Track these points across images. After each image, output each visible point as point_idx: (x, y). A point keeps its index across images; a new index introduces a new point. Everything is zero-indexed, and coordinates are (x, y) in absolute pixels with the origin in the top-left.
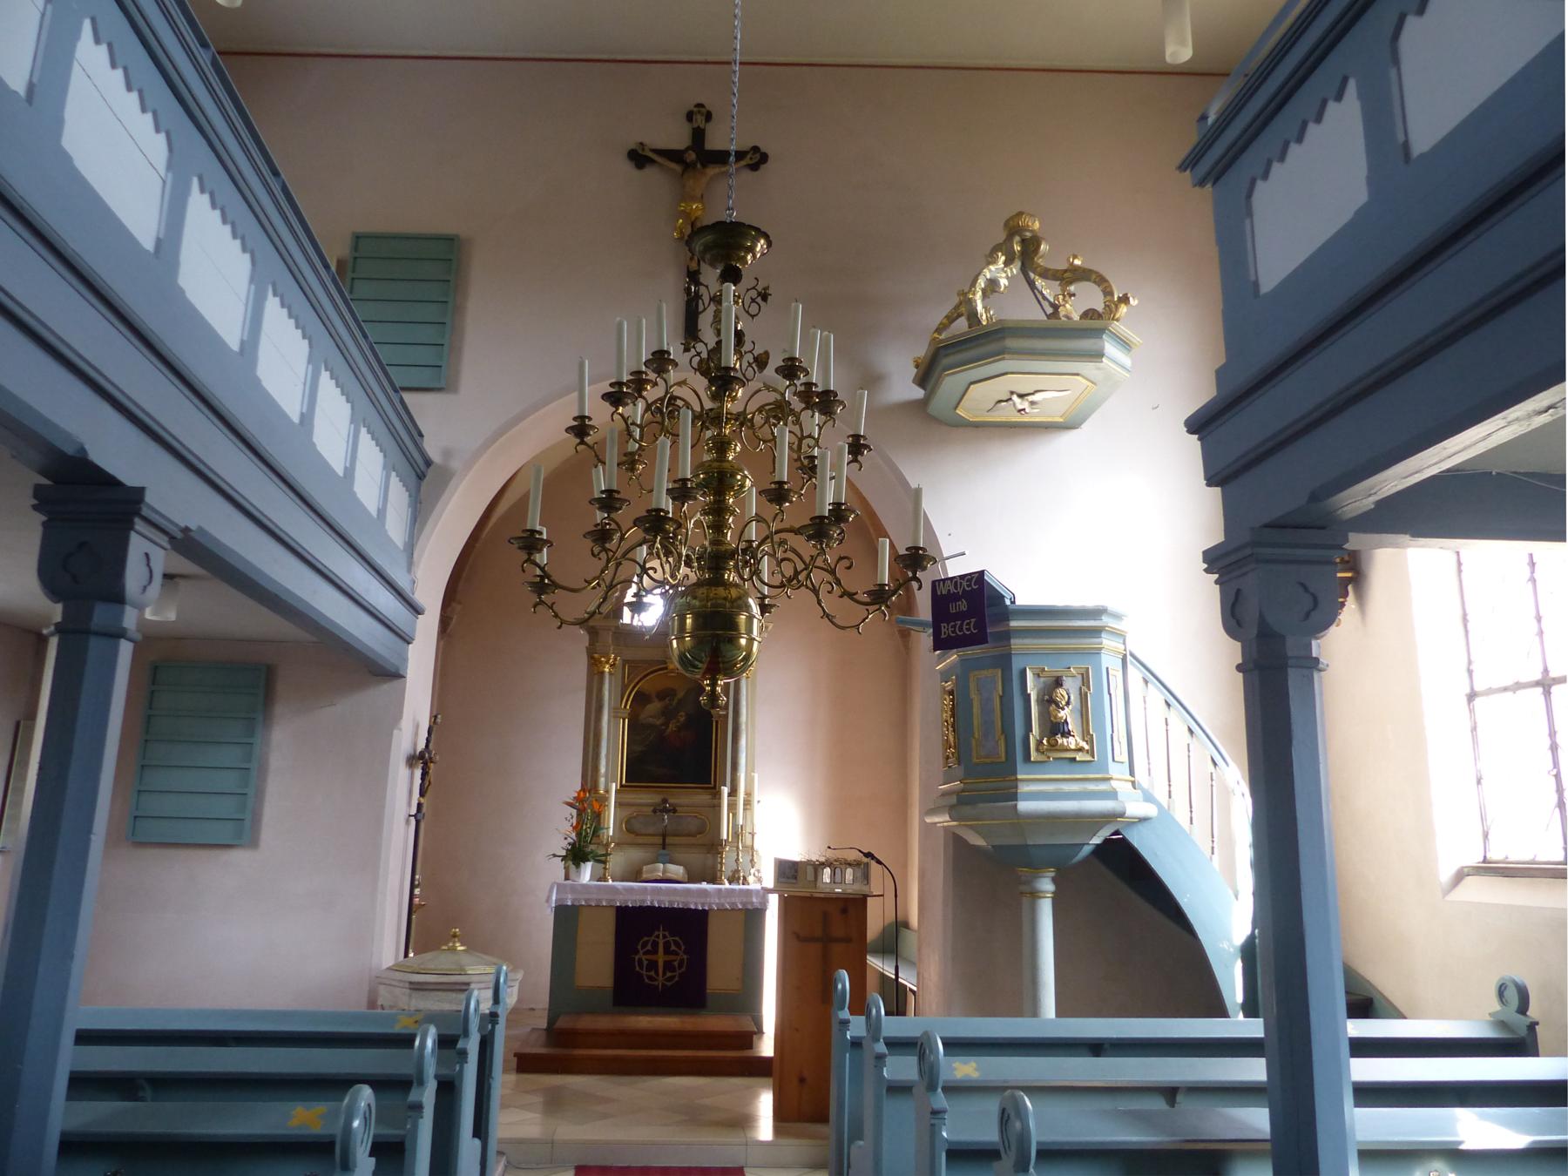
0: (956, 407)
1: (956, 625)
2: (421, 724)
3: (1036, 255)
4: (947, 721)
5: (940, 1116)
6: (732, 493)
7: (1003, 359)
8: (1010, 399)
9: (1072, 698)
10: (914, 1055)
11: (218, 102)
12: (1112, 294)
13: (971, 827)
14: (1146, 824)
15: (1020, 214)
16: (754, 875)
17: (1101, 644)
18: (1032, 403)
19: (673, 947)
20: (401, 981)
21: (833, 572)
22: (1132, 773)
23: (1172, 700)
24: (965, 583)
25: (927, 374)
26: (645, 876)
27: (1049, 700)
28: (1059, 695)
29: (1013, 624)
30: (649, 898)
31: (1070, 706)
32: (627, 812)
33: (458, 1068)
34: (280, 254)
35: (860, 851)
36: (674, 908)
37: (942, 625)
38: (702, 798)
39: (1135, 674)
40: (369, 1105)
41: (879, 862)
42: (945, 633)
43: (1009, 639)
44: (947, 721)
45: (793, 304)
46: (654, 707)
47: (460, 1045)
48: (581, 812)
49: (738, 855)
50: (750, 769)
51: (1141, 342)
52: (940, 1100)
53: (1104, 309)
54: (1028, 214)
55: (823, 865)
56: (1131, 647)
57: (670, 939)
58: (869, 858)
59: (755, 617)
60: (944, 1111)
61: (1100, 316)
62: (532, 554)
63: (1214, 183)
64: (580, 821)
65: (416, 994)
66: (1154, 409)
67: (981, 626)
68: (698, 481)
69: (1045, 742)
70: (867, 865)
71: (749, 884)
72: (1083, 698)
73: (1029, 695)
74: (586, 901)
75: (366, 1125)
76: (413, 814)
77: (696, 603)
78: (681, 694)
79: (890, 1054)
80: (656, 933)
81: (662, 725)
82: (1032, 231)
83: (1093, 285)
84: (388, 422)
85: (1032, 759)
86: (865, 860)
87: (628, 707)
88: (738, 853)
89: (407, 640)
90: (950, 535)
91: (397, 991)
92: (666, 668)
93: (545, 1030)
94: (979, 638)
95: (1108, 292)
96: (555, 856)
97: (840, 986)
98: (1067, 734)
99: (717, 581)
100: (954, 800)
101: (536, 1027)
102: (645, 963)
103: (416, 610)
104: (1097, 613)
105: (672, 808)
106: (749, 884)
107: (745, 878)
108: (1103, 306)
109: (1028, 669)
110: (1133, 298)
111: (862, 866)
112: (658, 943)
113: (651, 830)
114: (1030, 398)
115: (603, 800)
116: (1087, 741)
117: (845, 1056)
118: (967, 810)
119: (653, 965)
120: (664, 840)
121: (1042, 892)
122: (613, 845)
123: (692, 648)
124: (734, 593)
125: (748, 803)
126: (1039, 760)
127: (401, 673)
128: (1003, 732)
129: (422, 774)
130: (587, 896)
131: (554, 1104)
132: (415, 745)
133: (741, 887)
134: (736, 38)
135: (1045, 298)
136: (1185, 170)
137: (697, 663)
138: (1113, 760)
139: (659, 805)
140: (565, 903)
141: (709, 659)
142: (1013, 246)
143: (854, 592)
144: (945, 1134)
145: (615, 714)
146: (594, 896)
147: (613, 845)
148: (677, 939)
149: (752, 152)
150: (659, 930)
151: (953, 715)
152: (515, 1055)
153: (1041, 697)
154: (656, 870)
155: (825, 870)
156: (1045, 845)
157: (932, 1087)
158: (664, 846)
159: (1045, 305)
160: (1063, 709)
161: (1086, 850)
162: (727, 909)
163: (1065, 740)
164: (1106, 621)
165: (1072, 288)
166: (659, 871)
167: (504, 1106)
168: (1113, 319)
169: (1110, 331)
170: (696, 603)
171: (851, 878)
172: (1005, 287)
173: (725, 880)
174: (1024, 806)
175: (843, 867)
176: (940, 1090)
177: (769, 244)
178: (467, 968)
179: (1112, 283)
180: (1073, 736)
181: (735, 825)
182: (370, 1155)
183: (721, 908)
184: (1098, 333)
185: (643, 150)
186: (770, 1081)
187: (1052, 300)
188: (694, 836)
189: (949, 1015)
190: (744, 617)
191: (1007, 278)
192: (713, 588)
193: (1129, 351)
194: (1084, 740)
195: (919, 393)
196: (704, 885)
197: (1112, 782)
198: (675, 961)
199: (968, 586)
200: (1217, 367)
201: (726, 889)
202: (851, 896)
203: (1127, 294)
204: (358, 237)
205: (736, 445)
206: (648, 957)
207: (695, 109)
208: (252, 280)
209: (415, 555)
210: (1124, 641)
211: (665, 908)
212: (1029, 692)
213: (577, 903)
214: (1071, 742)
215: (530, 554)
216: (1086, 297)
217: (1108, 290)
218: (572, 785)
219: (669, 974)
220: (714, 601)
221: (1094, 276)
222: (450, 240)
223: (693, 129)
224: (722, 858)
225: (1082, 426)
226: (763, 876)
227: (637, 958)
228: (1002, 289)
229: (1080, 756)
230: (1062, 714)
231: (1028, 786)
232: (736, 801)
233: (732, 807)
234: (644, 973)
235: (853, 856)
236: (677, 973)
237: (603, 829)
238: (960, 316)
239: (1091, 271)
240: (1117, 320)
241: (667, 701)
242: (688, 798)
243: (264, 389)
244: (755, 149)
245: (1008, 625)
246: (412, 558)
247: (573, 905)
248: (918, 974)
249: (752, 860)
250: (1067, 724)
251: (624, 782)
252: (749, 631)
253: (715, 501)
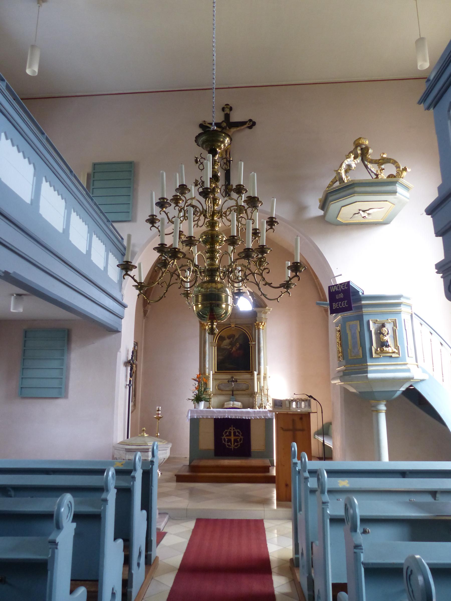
0: (337, 217)
1: (339, 303)
2: (129, 350)
3: (367, 154)
4: (338, 343)
5: (326, 504)
6: (218, 244)
7: (354, 196)
8: (359, 213)
10: (316, 477)
11: (9, 102)
12: (399, 167)
13: (349, 384)
14: (424, 382)
15: (360, 138)
16: (269, 405)
17: (401, 309)
18: (369, 214)
19: (237, 434)
20: (122, 448)
21: (261, 275)
22: (417, 362)
23: (433, 331)
24: (342, 287)
25: (324, 205)
26: (225, 406)
27: (379, 333)
28: (384, 330)
29: (363, 302)
30: (227, 415)
31: (389, 335)
32: (218, 382)
33: (132, 483)
34: (48, 167)
36: (236, 419)
37: (333, 304)
38: (247, 376)
39: (416, 321)
40: (70, 502)
44: (338, 343)
45: (240, 162)
46: (227, 342)
47: (132, 474)
48: (199, 382)
50: (266, 364)
51: (413, 186)
52: (326, 497)
53: (397, 174)
54: (363, 138)
55: (292, 401)
56: (414, 310)
57: (236, 430)
58: (311, 398)
59: (229, 295)
60: (328, 502)
61: (395, 177)
62: (128, 271)
63: (434, 108)
64: (199, 386)
65: (128, 453)
66: (421, 215)
67: (349, 303)
68: (203, 239)
69: (379, 349)
70: (310, 400)
72: (394, 332)
73: (371, 331)
74: (202, 417)
75: (69, 510)
76: (128, 384)
77: (203, 290)
78: (237, 337)
79: (310, 477)
80: (230, 428)
81: (230, 348)
82: (365, 145)
83: (392, 165)
84: (106, 234)
85: (374, 357)
86: (309, 398)
87: (216, 342)
88: (262, 397)
89: (121, 318)
90: (337, 269)
91: (121, 452)
92: (230, 327)
93: (188, 465)
94: (349, 308)
95: (398, 167)
96: (189, 399)
97: (293, 449)
98: (388, 346)
99: (212, 281)
100: (341, 374)
101: (185, 464)
102: (226, 440)
103: (124, 306)
104: (398, 297)
106: (266, 409)
107: (265, 407)
108: (396, 173)
109: (370, 321)
110: (409, 168)
113: (227, 389)
114: (368, 212)
115: (208, 378)
116: (396, 349)
117: (296, 477)
118: (347, 377)
119: (229, 441)
120: (233, 393)
122: (212, 395)
123: (202, 309)
124: (219, 286)
125: (265, 378)
126: (376, 357)
127: (119, 330)
128: (361, 346)
129: (130, 369)
130: (203, 414)
131: (192, 494)
132: (127, 358)
133: (264, 410)
134: (214, 55)
135: (372, 172)
136: (421, 104)
137: (205, 316)
138: (408, 356)
139: (230, 379)
141: (209, 314)
142: (357, 151)
143: (271, 283)
144: (328, 512)
145: (211, 344)
147: (212, 395)
148: (238, 430)
149: (249, 122)
150: (231, 427)
151: (340, 340)
152: (176, 475)
153: (376, 331)
155: (293, 403)
156: (380, 391)
157: (323, 492)
159: (373, 174)
160: (386, 336)
161: (398, 393)
163: (387, 349)
164: (402, 300)
165: (383, 167)
166: (231, 404)
167: (161, 495)
168: (400, 177)
169: (399, 182)
170: (203, 290)
171: (304, 406)
172: (355, 167)
174: (370, 375)
175: (300, 401)
176: (326, 493)
177: (231, 140)
178: (148, 443)
179: (399, 163)
180: (391, 347)
181: (260, 386)
182: (73, 521)
184: (394, 183)
185: (205, 123)
186: (274, 485)
187: (375, 173)
188: (245, 391)
189: (345, 460)
190: (224, 295)
191: (356, 164)
192: (210, 284)
193: (408, 190)
194: (395, 348)
195: (321, 213)
196: (249, 410)
198: (238, 439)
199: (343, 288)
200: (438, 186)
201: (257, 411)
203: (405, 167)
204: (95, 164)
205: (219, 224)
206: (228, 437)
207: (225, 106)
208: (35, 175)
209: (123, 285)
210: (411, 308)
211: (233, 419)
212: (371, 330)
213: (198, 417)
214: (390, 349)
215: (127, 272)
216: (390, 169)
217: (398, 166)
218: (196, 372)
219: (236, 444)
220: (210, 289)
221: (392, 161)
222: (131, 163)
223: (225, 114)
224: (255, 399)
225: (391, 223)
226: (269, 407)
227: (223, 438)
228: (353, 169)
229: (394, 355)
230: (386, 338)
231: (372, 367)
232: (260, 377)
233: (259, 379)
234: (226, 443)
235: (304, 397)
237: (207, 389)
238: (337, 181)
239: (390, 159)
240: (402, 178)
241: (231, 339)
242: (242, 376)
243: (43, 217)
244: (250, 120)
245: (361, 303)
246: (122, 286)
247: (197, 418)
248: (333, 443)
249: (268, 400)
250: (388, 342)
251: (216, 371)
252: (227, 301)
253: (210, 248)
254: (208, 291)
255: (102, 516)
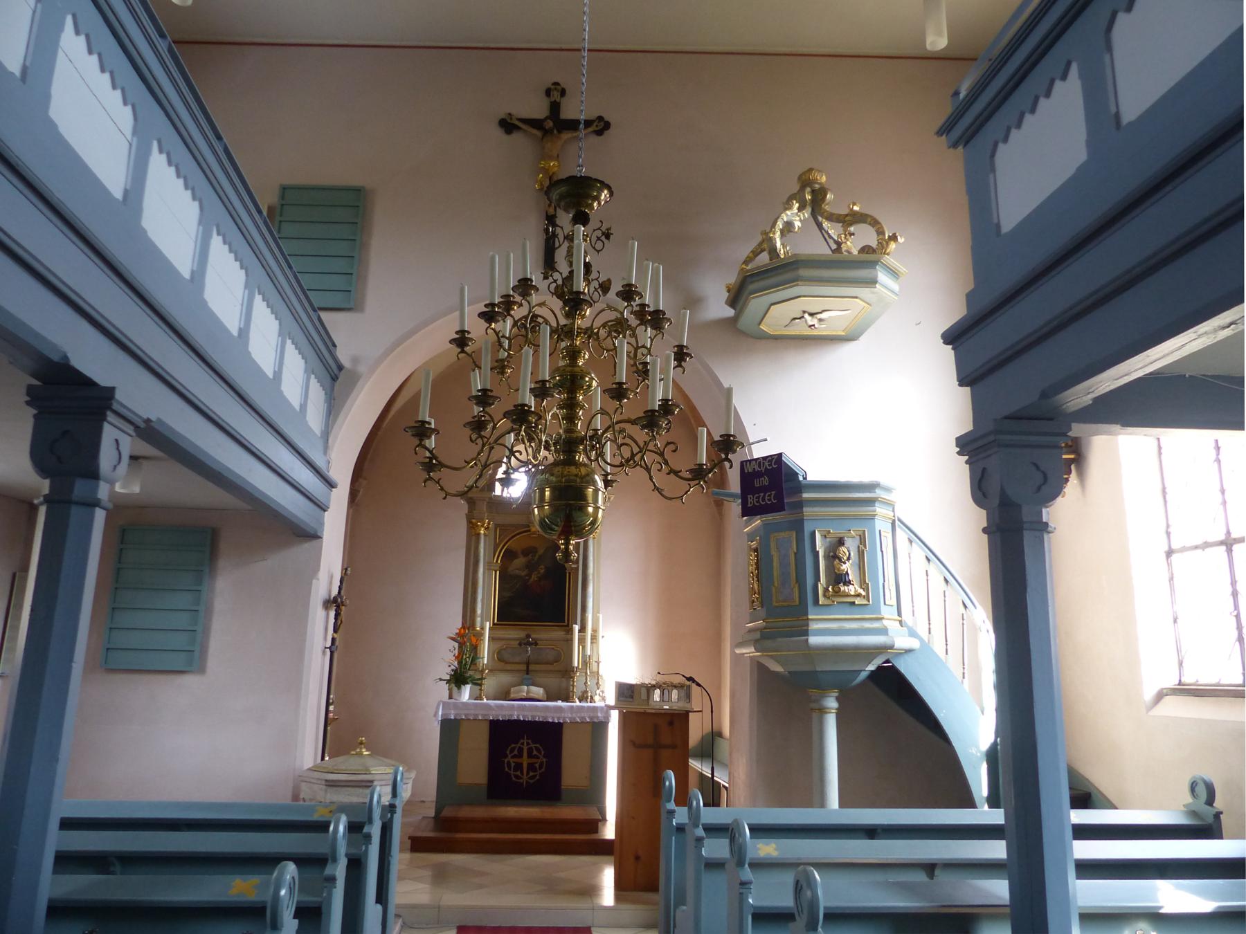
0: (760, 324)
1: (760, 496)
2: (334, 575)
3: (823, 203)
4: (752, 573)
5: (747, 886)
6: (582, 392)
7: (797, 285)
8: (803, 317)
9: (852, 554)
11: (173, 81)
12: (883, 234)
13: (772, 657)
14: (911, 654)
15: (811, 170)
16: (599, 695)
17: (875, 511)
18: (820, 320)
19: (535, 752)
20: (318, 779)
22: (899, 614)
23: (932, 556)
24: (767, 463)
25: (737, 297)
26: (512, 696)
27: (833, 556)
28: (842, 552)
29: (805, 495)
30: (516, 713)
31: (851, 561)
32: (498, 645)
34: (223, 202)
35: (683, 676)
36: (535, 721)
37: (749, 496)
38: (558, 634)
39: (902, 535)
40: (293, 878)
41: (698, 685)
42: (751, 503)
43: (802, 508)
44: (752, 573)
45: (630, 242)
46: (520, 561)
47: (366, 830)
49: (586, 679)
50: (596, 611)
51: (907, 271)
52: (747, 874)
53: (878, 245)
54: (817, 170)
55: (654, 687)
56: (899, 514)
57: (532, 745)
58: (691, 682)
59: (600, 490)
60: (750, 883)
61: (874, 251)
62: (423, 440)
63: (965, 146)
64: (461, 652)
65: (330, 789)
66: (917, 324)
67: (780, 497)
68: (555, 382)
69: (830, 589)
70: (689, 687)
71: (595, 702)
72: (861, 554)
73: (818, 552)
74: (465, 716)
75: (291, 894)
76: (328, 646)
77: (553, 479)
78: (541, 552)
79: (707, 837)
80: (522, 741)
81: (526, 576)
82: (820, 184)
83: (869, 226)
84: (308, 335)
85: (820, 603)
86: (688, 683)
87: (499, 562)
88: (586, 677)
90: (755, 425)
91: (316, 787)
92: (529, 531)
93: (433, 818)
94: (778, 507)
95: (880, 232)
96: (441, 679)
97: (667, 783)
98: (848, 583)
99: (570, 461)
100: (758, 635)
101: (426, 815)
102: (513, 765)
103: (331, 485)
104: (872, 487)
105: (534, 642)
107: (592, 697)
108: (876, 243)
109: (817, 532)
110: (901, 236)
111: (685, 688)
112: (523, 749)
113: (517, 659)
114: (819, 316)
115: (479, 636)
116: (863, 589)
117: (672, 839)
118: (768, 643)
119: (519, 767)
120: (528, 667)
121: (828, 708)
122: (487, 671)
123: (550, 515)
124: (583, 471)
125: (594, 638)
126: (825, 603)
127: (319, 534)
128: (797, 581)
129: (335, 615)
130: (466, 712)
131: (440, 877)
132: (330, 591)
133: (589, 704)
134: (585, 30)
135: (830, 237)
136: (942, 135)
137: (554, 526)
138: (885, 604)
139: (524, 639)
140: (449, 717)
141: (563, 523)
142: (805, 195)
143: (679, 470)
144: (751, 901)
145: (489, 567)
146: (472, 712)
147: (487, 671)
148: (538, 745)
149: (597, 121)
151: (757, 568)
152: (410, 838)
153: (827, 553)
154: (521, 691)
155: (655, 691)
156: (830, 671)
157: (740, 863)
158: (528, 672)
159: (831, 242)
160: (845, 563)
161: (863, 675)
162: (578, 722)
163: (846, 588)
164: (879, 493)
165: (852, 229)
166: (523, 692)
167: (401, 878)
168: (884, 253)
169: (882, 263)
170: (553, 479)
171: (677, 697)
172: (799, 228)
173: (576, 699)
174: (814, 640)
175: (670, 688)
176: (747, 866)
177: (611, 194)
178: (371, 769)
179: (883, 225)
180: (853, 585)
181: (584, 655)
182: (294, 918)
183: (573, 721)
184: (872, 264)
185: (511, 119)
186: (612, 858)
187: (836, 238)
189: (754, 806)
190: (591, 490)
191: (800, 220)
192: (567, 467)
193: (897, 278)
194: (861, 588)
195: (730, 312)
196: (560, 703)
197: (884, 621)
198: (537, 763)
199: (769, 465)
200: (967, 291)
201: (577, 706)
202: (676, 712)
203: (895, 234)
204: (284, 189)
205: (585, 354)
206: (515, 760)
207: (553, 87)
208: (200, 222)
209: (330, 441)
210: (893, 509)
211: (529, 721)
212: (817, 549)
213: (458, 717)
214: (851, 590)
215: (421, 440)
216: (863, 236)
217: (881, 230)
218: (454, 623)
219: (531, 774)
220: (567, 477)
221: (869, 220)
222: (358, 191)
223: (551, 102)
224: (573, 681)
225: (860, 338)
226: (607, 695)
227: (506, 761)
228: (796, 230)
229: (858, 601)
230: (844, 567)
231: (817, 624)
232: (585, 636)
233: (582, 641)
234: (512, 772)
235: (678, 680)
236: (538, 773)
237: (479, 658)
238: (762, 251)
239: (867, 215)
240: (888, 254)
241: (530, 557)
242: (547, 634)
243: (210, 309)
244: (600, 118)
245: (801, 496)
246: (328, 443)
247: (455, 719)
248: (730, 774)
249: (598, 683)
250: (848, 575)
251: (496, 621)
252: (596, 501)
253: (568, 398)
254: (564, 480)
255: (324, 910)
